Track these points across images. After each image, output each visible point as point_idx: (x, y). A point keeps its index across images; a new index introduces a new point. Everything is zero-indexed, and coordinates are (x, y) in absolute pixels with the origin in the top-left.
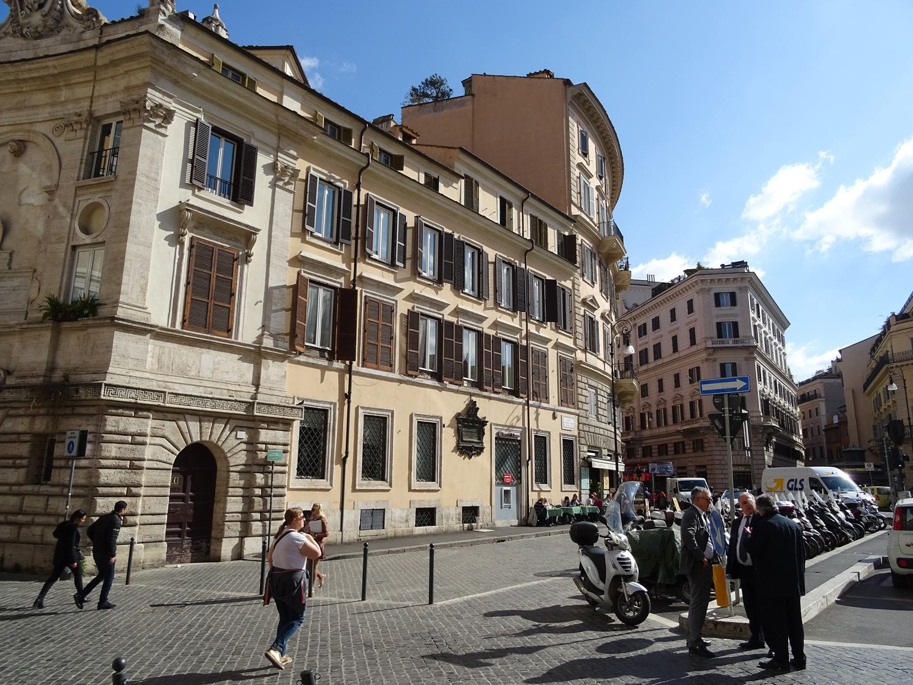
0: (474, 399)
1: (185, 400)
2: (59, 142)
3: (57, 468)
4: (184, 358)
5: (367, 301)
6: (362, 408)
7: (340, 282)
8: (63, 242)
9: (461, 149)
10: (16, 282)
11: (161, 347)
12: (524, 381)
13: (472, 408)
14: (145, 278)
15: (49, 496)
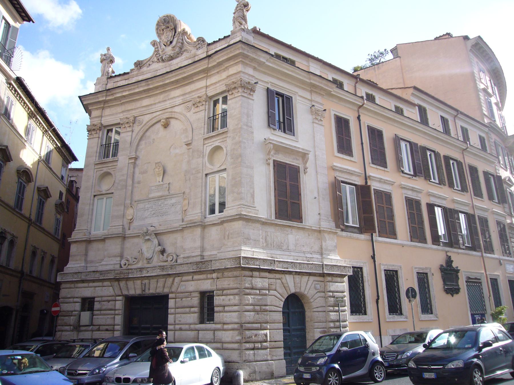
0: (449, 254)
1: (285, 265)
2: (188, 115)
3: (217, 312)
4: (279, 238)
5: (377, 191)
6: (383, 265)
7: (359, 181)
8: (200, 172)
9: (415, 88)
10: (173, 201)
11: (266, 232)
12: (479, 240)
13: (449, 261)
14: (253, 188)
15: (215, 330)
